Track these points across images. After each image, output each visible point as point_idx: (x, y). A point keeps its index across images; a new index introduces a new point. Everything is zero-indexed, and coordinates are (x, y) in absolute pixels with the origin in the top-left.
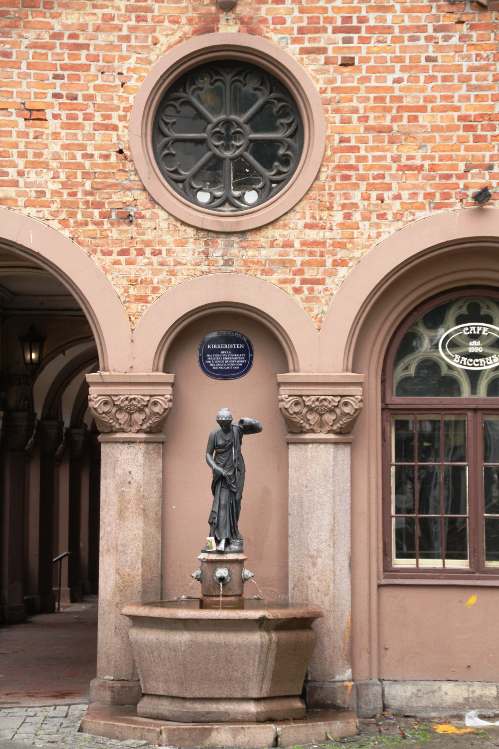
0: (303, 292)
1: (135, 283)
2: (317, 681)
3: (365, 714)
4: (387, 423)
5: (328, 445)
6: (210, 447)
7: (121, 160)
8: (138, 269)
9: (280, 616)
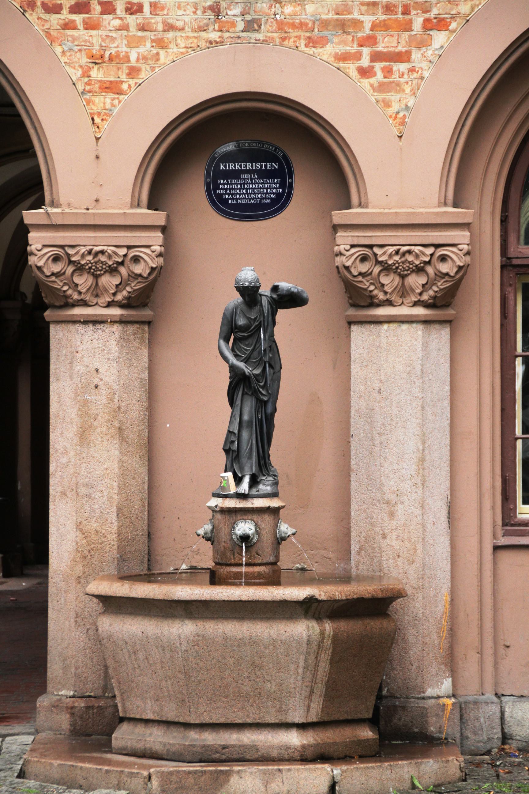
0: (375, 74)
1: (100, 61)
2: (397, 698)
3: (473, 748)
4: (509, 289)
5: (414, 325)
6: (225, 328)
8: (104, 37)
9: (338, 596)
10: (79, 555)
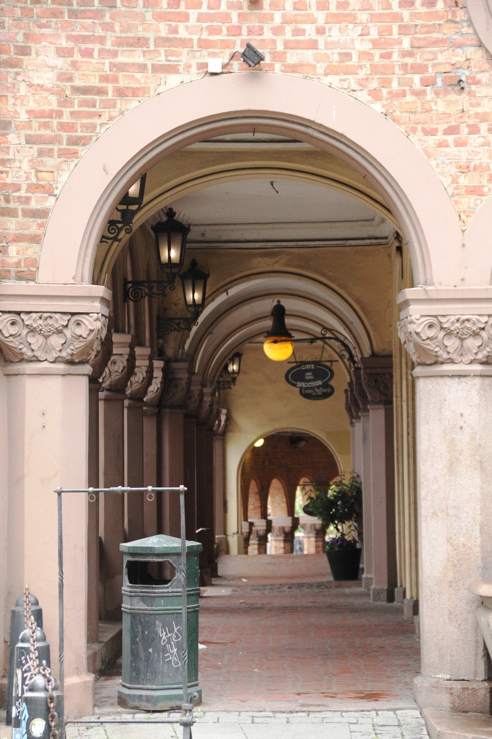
1: (466, 171)
7: (450, 7)
8: (470, 152)
10: (450, 564)
